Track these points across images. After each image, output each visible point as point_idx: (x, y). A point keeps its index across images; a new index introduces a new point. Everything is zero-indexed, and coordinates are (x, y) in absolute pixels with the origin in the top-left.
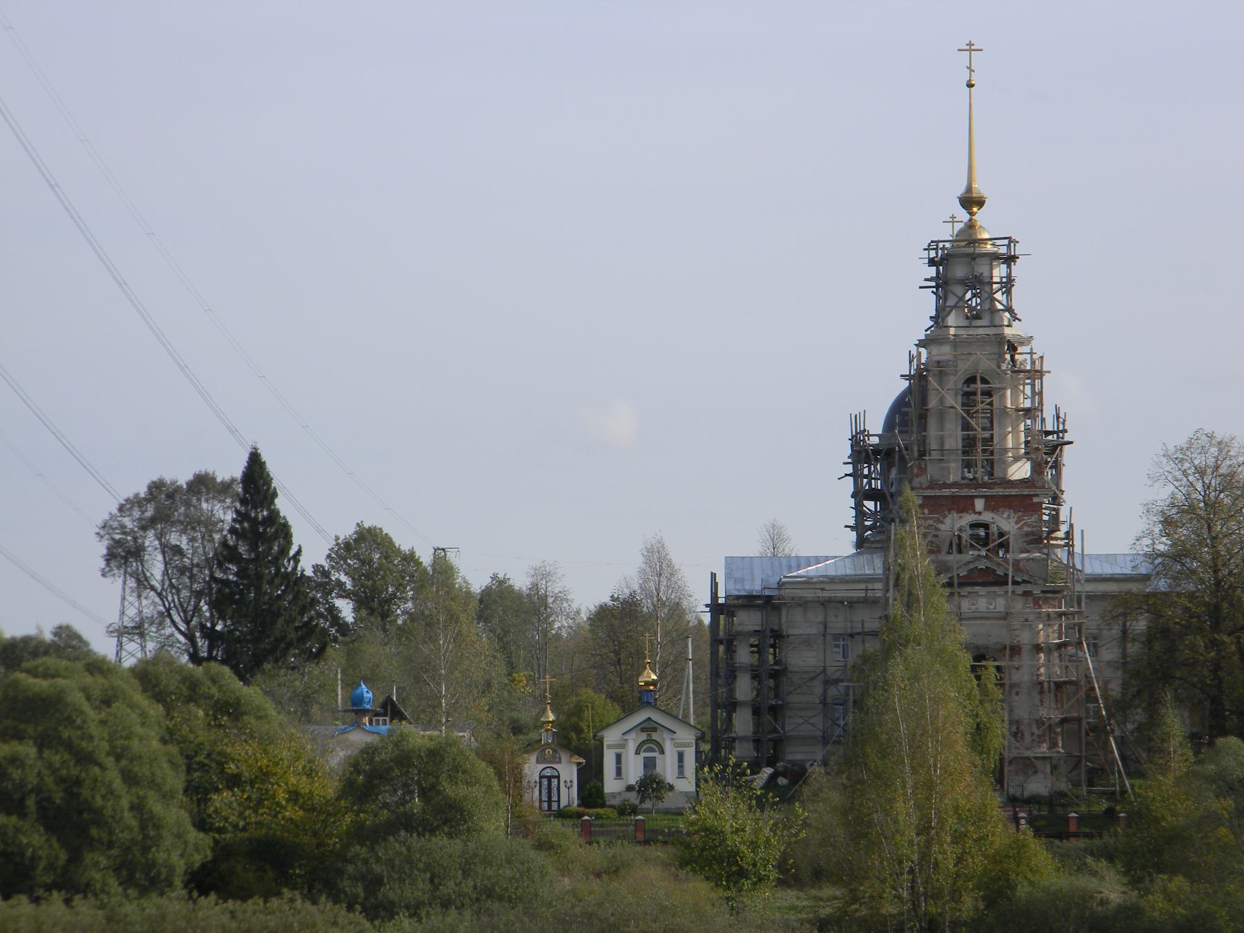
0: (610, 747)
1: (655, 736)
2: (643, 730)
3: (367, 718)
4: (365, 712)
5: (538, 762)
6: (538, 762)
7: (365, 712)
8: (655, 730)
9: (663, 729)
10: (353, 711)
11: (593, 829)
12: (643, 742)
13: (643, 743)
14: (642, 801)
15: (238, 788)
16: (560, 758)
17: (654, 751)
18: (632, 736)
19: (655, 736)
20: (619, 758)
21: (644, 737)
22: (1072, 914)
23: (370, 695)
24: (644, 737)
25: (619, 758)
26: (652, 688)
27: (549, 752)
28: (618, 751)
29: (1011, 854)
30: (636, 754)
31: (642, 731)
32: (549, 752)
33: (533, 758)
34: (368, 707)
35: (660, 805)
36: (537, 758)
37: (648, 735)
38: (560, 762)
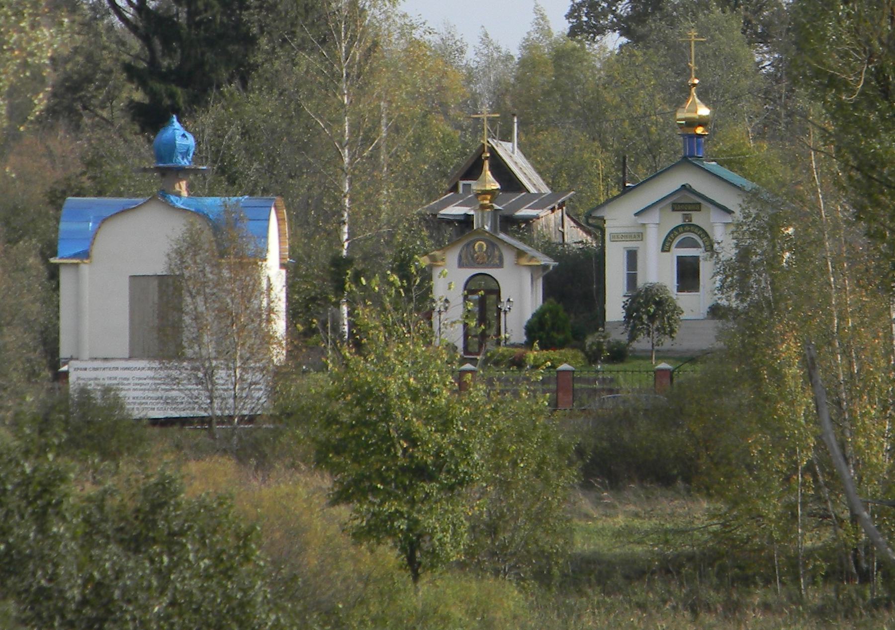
0: (616, 238)
1: (697, 219)
2: (676, 207)
3: (183, 184)
4: (180, 172)
5: (461, 265)
6: (461, 265)
7: (180, 172)
8: (697, 207)
9: (711, 206)
10: (157, 169)
11: (577, 386)
12: (676, 229)
13: (676, 230)
14: (632, 338)
15: (341, 252)
16: (501, 259)
17: (695, 245)
18: (654, 217)
19: (697, 219)
20: (632, 257)
21: (677, 219)
22: (94, 614)
23: (191, 141)
24: (677, 219)
25: (632, 257)
26: (700, 130)
27: (481, 247)
28: (631, 245)
29: (57, 528)
30: (663, 250)
31: (674, 210)
32: (481, 247)
33: (452, 257)
34: (185, 163)
35: (667, 343)
36: (460, 257)
37: (687, 217)
38: (500, 265)
